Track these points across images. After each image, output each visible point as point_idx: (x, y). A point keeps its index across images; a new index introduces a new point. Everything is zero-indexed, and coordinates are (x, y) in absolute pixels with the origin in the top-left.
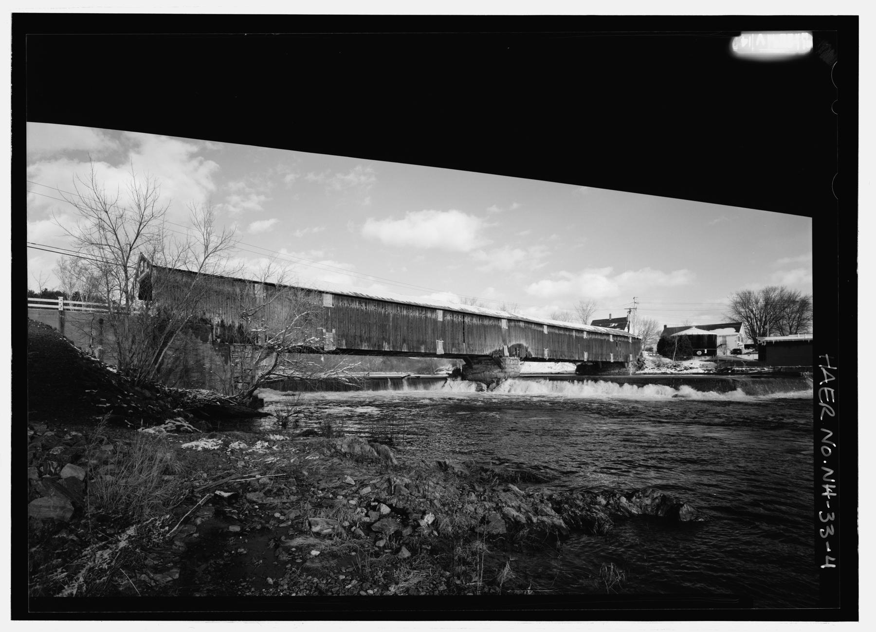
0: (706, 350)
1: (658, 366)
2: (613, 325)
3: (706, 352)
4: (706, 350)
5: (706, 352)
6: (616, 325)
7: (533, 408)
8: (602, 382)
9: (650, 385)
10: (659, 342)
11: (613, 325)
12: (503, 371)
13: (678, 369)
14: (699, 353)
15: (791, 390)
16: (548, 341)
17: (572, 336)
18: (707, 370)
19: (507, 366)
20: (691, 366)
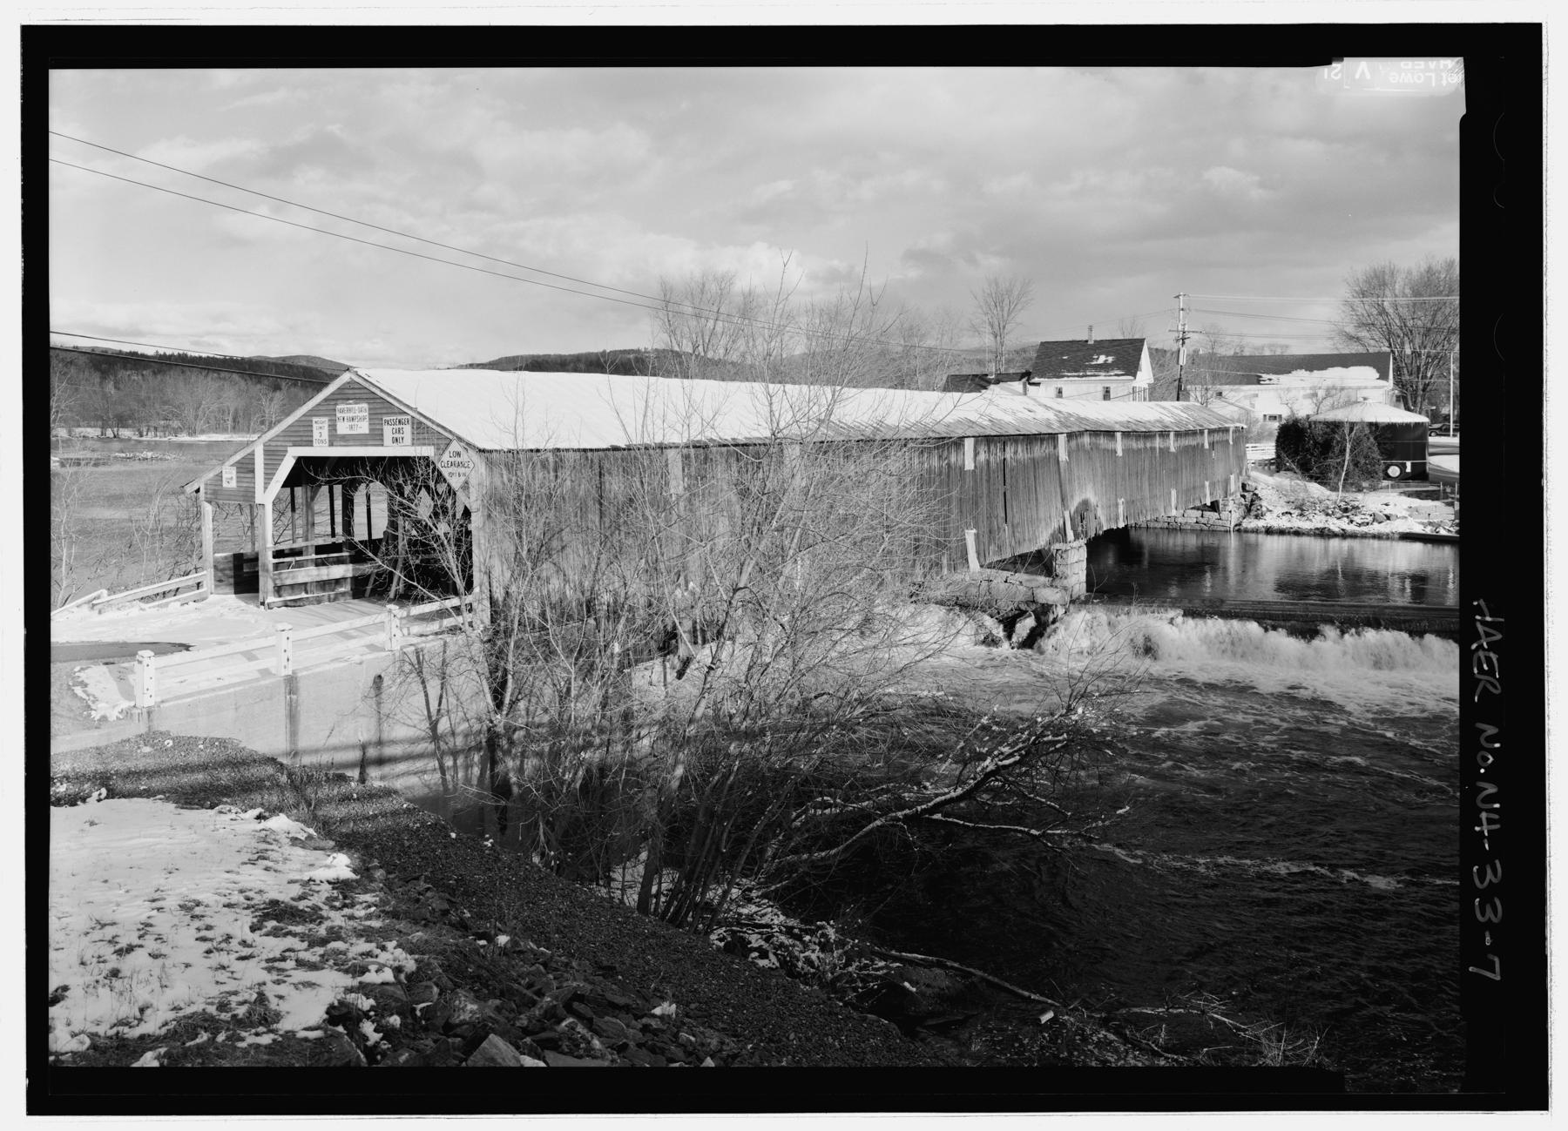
0: (1409, 464)
1: (1301, 509)
2: (1102, 359)
3: (1409, 470)
4: (1409, 464)
5: (1409, 470)
6: (1110, 359)
7: (309, 641)
8: (1330, 632)
9: (1451, 641)
10: (1278, 438)
11: (1102, 359)
12: (1057, 582)
13: (1358, 519)
14: (1394, 471)
15: (1458, 382)
16: (1123, 479)
17: (1153, 449)
18: (1430, 524)
19: (1069, 572)
20: (1388, 511)
